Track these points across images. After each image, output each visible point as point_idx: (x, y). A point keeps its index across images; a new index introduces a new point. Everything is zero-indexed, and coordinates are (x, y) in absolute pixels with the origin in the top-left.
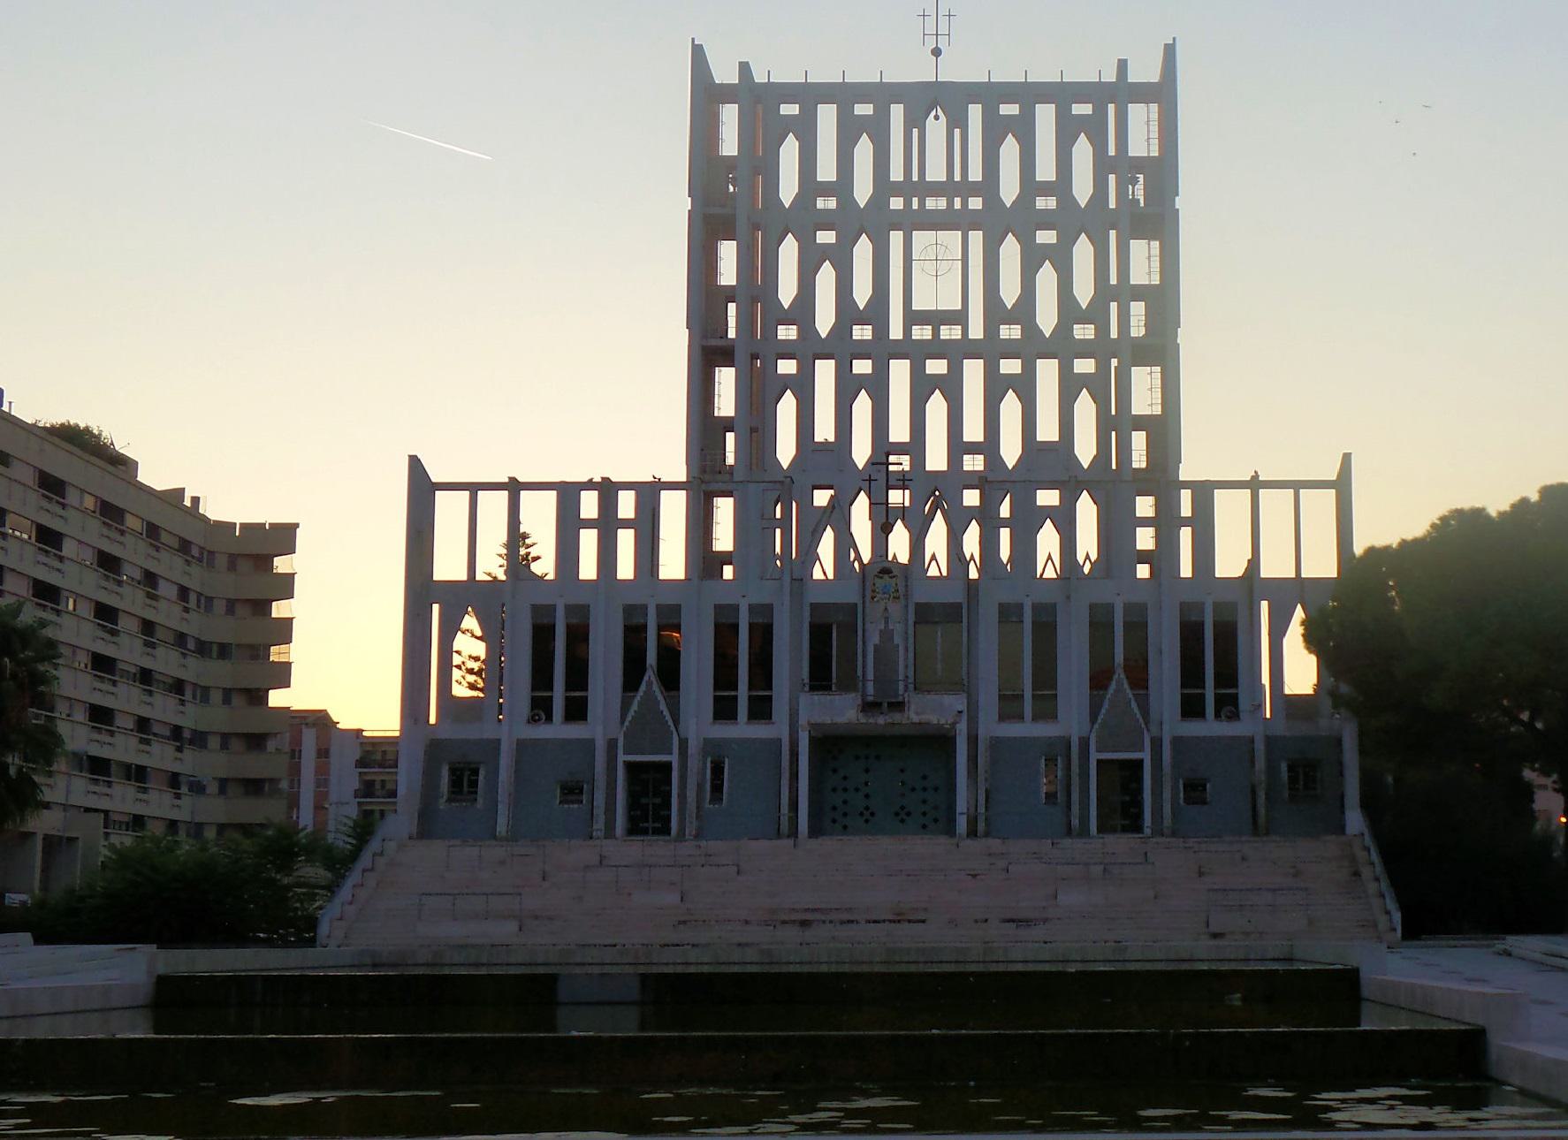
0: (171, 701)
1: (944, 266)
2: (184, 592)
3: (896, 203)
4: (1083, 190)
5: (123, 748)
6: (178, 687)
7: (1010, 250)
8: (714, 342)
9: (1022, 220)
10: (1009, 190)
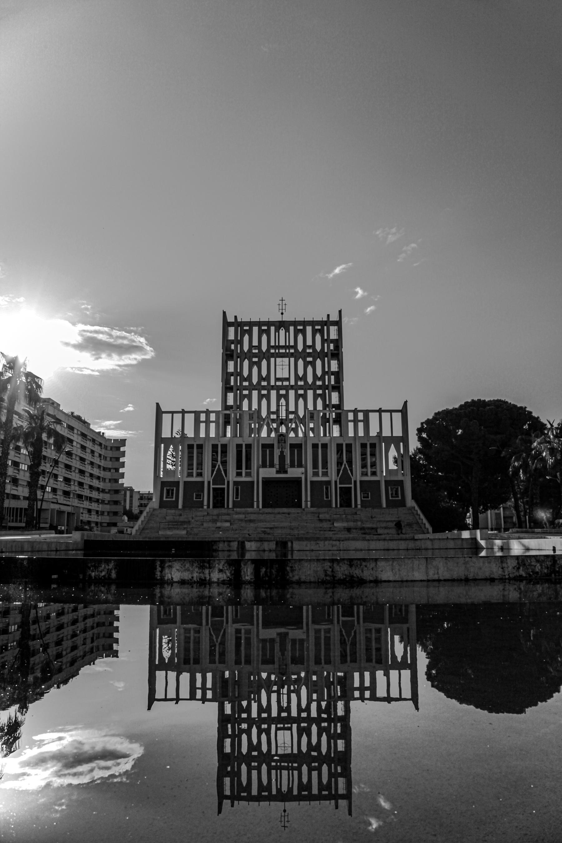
0: (97, 482)
1: (284, 367)
2: (100, 455)
3: (272, 351)
4: (318, 347)
5: (86, 492)
6: (98, 478)
7: (301, 363)
8: (228, 386)
9: (303, 355)
10: (300, 347)
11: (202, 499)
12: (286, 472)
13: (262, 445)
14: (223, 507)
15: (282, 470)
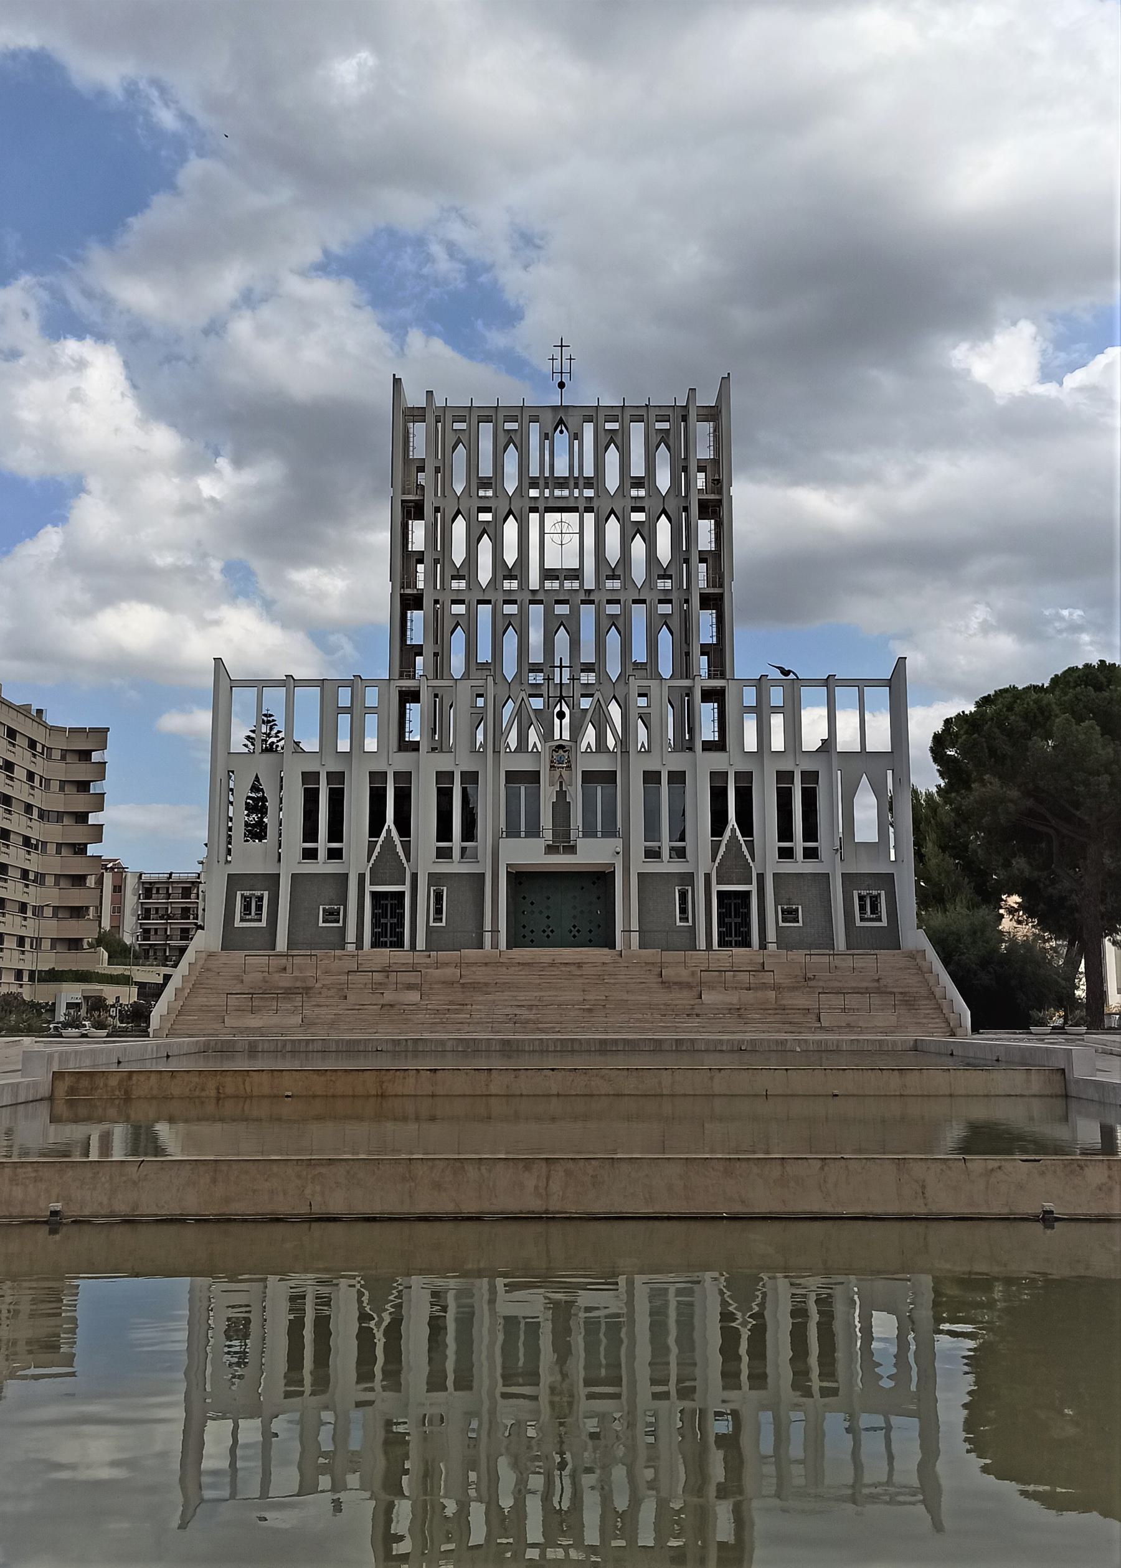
1: (567, 538)
2: (31, 776)
7: (613, 528)
8: (408, 591)
11: (341, 924)
12: (572, 849)
13: (508, 774)
14: (400, 944)
15: (563, 843)
